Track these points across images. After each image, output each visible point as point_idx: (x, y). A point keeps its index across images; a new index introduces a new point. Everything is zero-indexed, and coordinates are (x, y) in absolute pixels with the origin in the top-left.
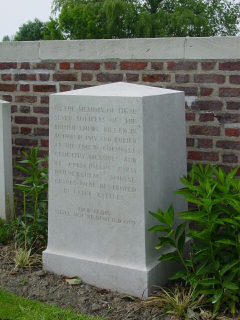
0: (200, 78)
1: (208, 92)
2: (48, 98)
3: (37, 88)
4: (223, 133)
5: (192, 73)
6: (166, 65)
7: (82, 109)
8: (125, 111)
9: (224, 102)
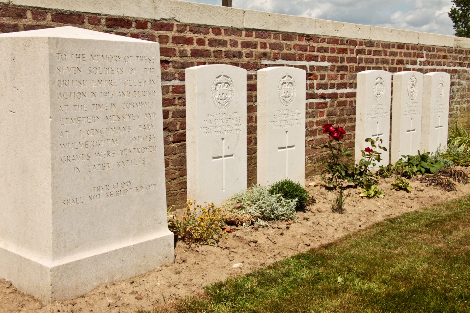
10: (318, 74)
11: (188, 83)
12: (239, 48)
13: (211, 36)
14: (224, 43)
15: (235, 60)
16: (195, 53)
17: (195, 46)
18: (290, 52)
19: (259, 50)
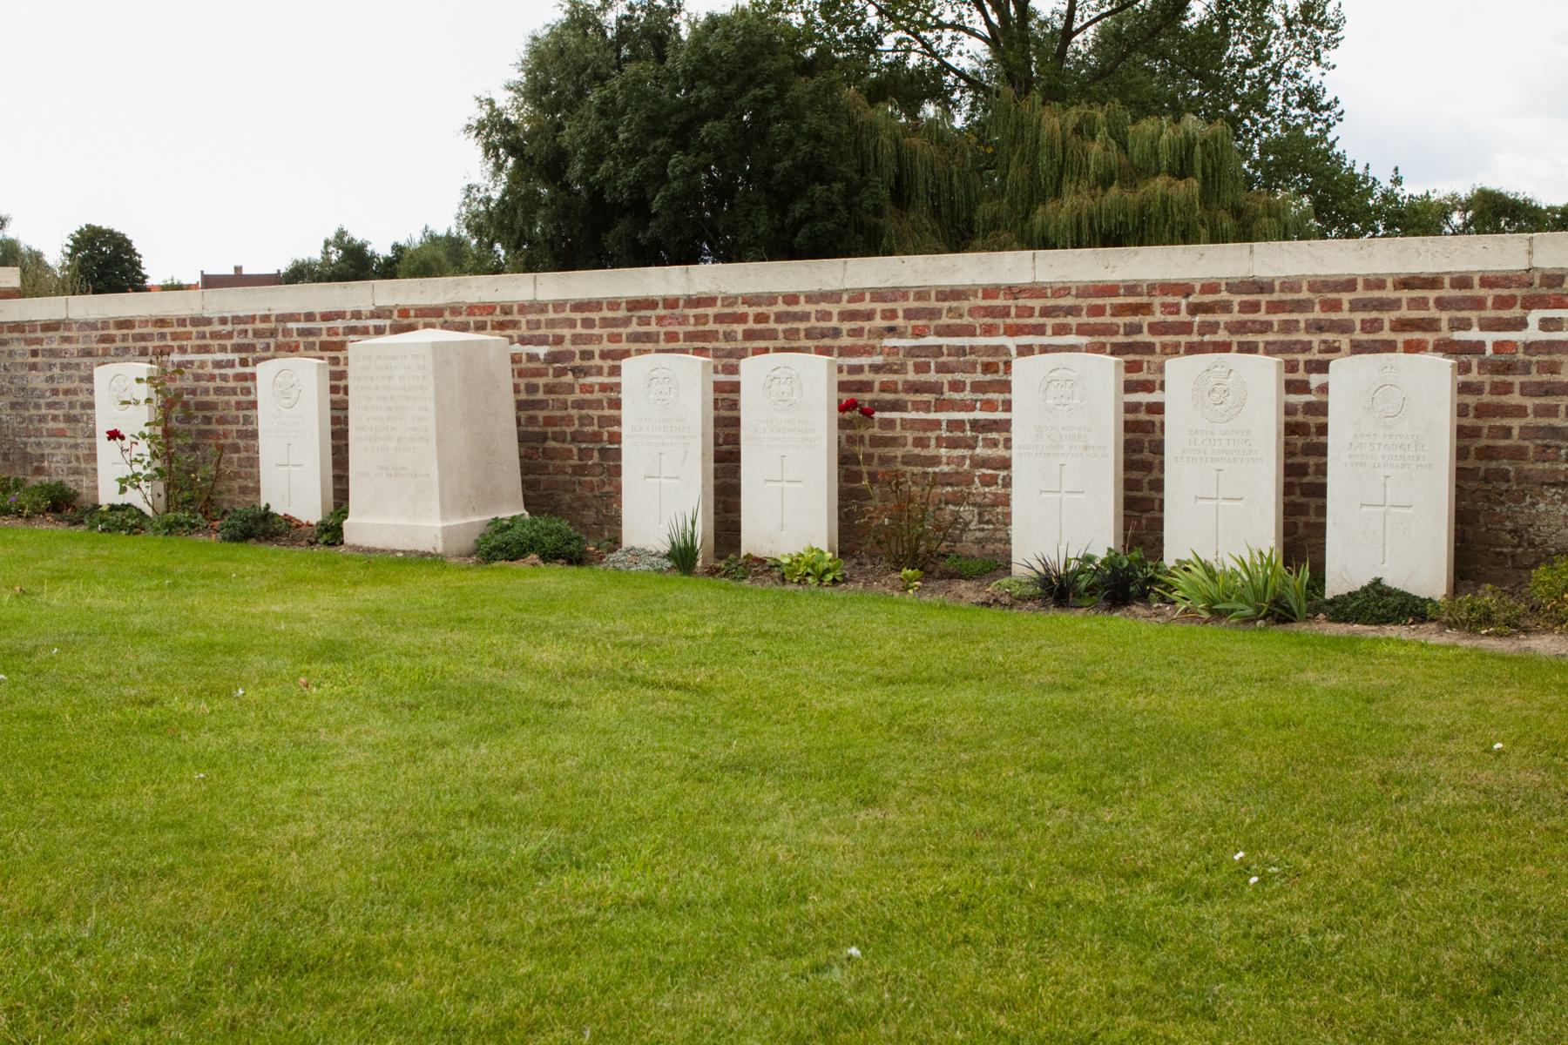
0: (551, 323)
1: (559, 340)
2: (619, 368)
3: (605, 355)
4: (577, 390)
5: (543, 317)
6: (515, 309)
7: (379, 357)
8: (416, 357)
9: (968, 381)
10: (597, 361)
11: (1023, 418)
12: (835, 323)
13: (781, 307)
14: (805, 317)
15: (827, 342)
16: (749, 335)
17: (751, 325)
18: (958, 321)
19: (879, 322)
